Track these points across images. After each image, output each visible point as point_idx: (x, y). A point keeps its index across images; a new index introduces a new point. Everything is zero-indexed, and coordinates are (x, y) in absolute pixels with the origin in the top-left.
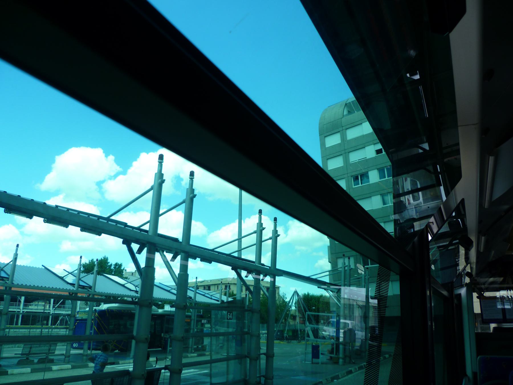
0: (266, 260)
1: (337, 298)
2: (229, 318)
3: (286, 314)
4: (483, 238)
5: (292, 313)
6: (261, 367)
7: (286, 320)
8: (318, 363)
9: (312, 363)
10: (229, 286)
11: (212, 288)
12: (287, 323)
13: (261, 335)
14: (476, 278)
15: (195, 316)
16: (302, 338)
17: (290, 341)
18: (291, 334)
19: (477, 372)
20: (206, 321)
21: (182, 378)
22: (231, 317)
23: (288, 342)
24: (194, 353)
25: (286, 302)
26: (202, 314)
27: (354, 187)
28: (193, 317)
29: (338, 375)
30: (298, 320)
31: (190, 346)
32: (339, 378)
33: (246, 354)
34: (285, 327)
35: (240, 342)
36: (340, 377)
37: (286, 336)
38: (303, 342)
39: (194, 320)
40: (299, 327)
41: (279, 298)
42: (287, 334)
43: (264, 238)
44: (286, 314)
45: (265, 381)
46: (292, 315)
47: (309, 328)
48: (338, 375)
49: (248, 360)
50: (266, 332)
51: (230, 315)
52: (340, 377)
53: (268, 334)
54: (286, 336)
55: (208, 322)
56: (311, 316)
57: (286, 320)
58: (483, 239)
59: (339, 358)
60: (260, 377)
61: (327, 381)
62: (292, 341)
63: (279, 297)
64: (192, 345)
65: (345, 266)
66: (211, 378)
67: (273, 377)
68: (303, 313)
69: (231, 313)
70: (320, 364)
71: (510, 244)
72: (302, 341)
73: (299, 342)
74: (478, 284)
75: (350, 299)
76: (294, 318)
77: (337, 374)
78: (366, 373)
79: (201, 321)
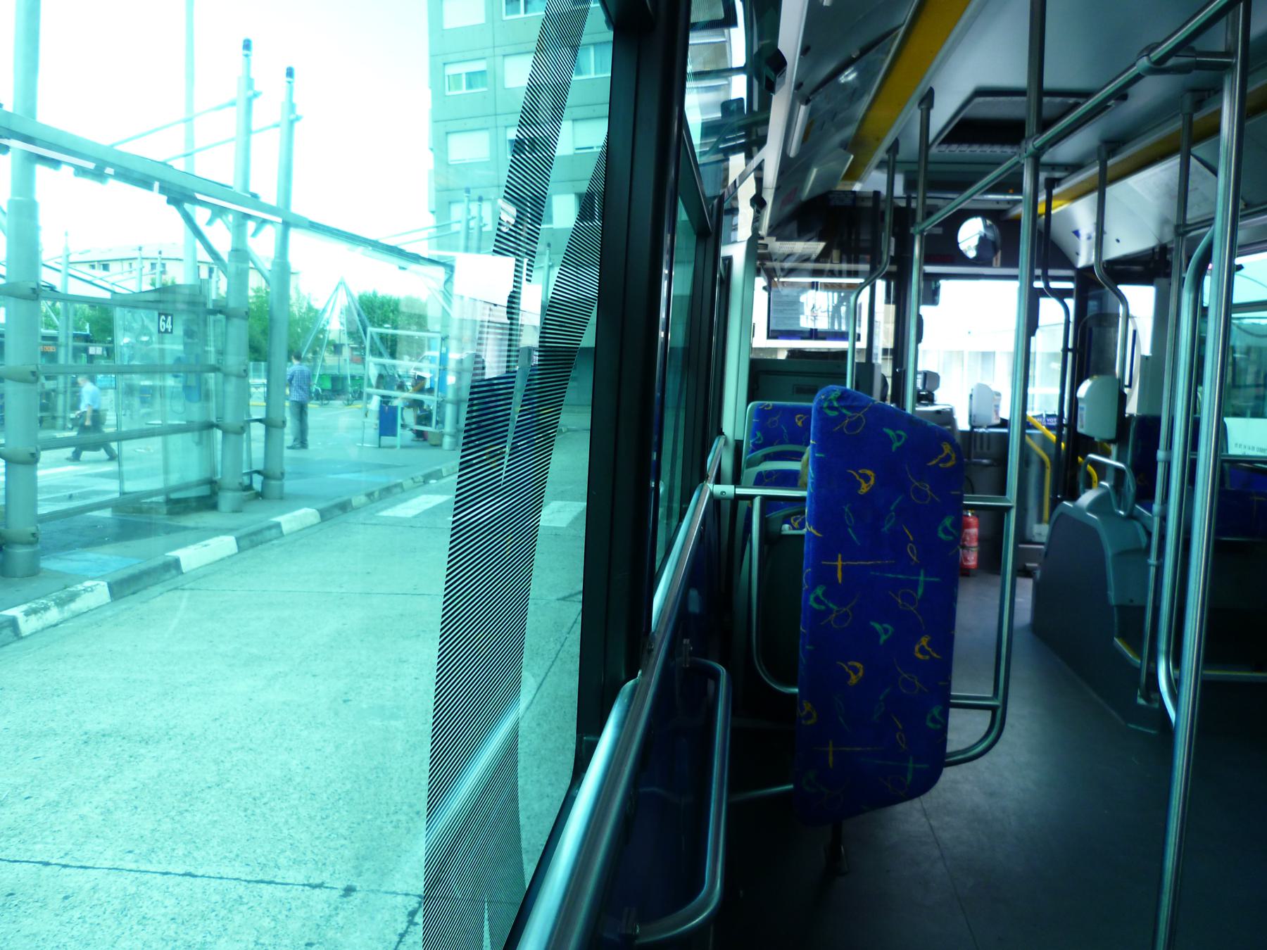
0: (267, 190)
1: (444, 294)
2: (163, 330)
3: (317, 339)
4: (803, 108)
5: (331, 338)
6: (254, 456)
7: (315, 353)
8: (393, 447)
9: (380, 447)
10: (164, 265)
11: (112, 266)
12: (319, 362)
13: (253, 390)
14: (767, 240)
15: (67, 337)
16: (357, 395)
17: (326, 402)
18: (328, 385)
19: (743, 441)
20: (101, 349)
21: (40, 483)
22: (169, 327)
23: (322, 405)
24: (71, 429)
25: (317, 311)
26: (88, 332)
27: (505, 18)
28: (62, 340)
29: (440, 471)
30: (346, 352)
31: (60, 412)
32: (443, 477)
33: (214, 420)
34: (314, 368)
35: (195, 391)
36: (444, 474)
37: (317, 390)
38: (359, 405)
39: (67, 346)
40: (349, 370)
41: (298, 300)
42: (319, 384)
43: (255, 125)
44: (317, 339)
45: (264, 485)
46: (330, 343)
47: (372, 367)
48: (440, 471)
49: (218, 434)
50: (265, 381)
51: (165, 321)
52: (444, 475)
53: (268, 386)
54: (317, 390)
55: (108, 354)
56: (375, 337)
57: (315, 353)
58: (803, 110)
59: (442, 435)
60: (250, 474)
61: (414, 482)
62: (331, 402)
63: (299, 297)
64: (65, 411)
65: (470, 217)
66: (122, 482)
67: (283, 474)
68: (361, 337)
69: (170, 318)
70: (399, 447)
71: (852, 157)
72: (355, 402)
73: (348, 405)
74: (768, 257)
75: (475, 300)
76: (337, 348)
77: (438, 468)
78: (505, 434)
79: (86, 350)
